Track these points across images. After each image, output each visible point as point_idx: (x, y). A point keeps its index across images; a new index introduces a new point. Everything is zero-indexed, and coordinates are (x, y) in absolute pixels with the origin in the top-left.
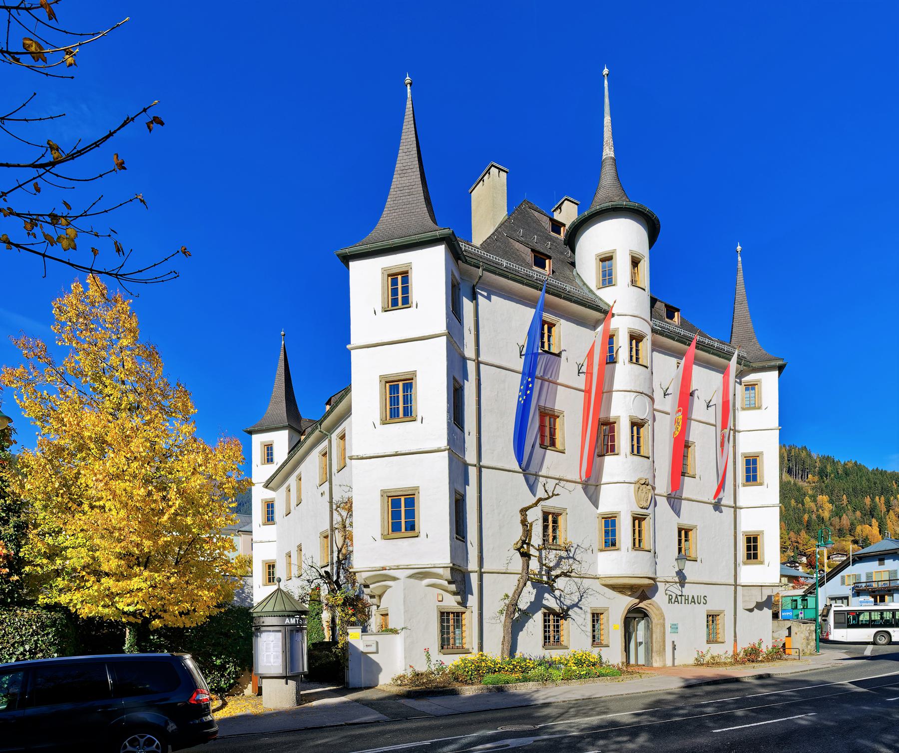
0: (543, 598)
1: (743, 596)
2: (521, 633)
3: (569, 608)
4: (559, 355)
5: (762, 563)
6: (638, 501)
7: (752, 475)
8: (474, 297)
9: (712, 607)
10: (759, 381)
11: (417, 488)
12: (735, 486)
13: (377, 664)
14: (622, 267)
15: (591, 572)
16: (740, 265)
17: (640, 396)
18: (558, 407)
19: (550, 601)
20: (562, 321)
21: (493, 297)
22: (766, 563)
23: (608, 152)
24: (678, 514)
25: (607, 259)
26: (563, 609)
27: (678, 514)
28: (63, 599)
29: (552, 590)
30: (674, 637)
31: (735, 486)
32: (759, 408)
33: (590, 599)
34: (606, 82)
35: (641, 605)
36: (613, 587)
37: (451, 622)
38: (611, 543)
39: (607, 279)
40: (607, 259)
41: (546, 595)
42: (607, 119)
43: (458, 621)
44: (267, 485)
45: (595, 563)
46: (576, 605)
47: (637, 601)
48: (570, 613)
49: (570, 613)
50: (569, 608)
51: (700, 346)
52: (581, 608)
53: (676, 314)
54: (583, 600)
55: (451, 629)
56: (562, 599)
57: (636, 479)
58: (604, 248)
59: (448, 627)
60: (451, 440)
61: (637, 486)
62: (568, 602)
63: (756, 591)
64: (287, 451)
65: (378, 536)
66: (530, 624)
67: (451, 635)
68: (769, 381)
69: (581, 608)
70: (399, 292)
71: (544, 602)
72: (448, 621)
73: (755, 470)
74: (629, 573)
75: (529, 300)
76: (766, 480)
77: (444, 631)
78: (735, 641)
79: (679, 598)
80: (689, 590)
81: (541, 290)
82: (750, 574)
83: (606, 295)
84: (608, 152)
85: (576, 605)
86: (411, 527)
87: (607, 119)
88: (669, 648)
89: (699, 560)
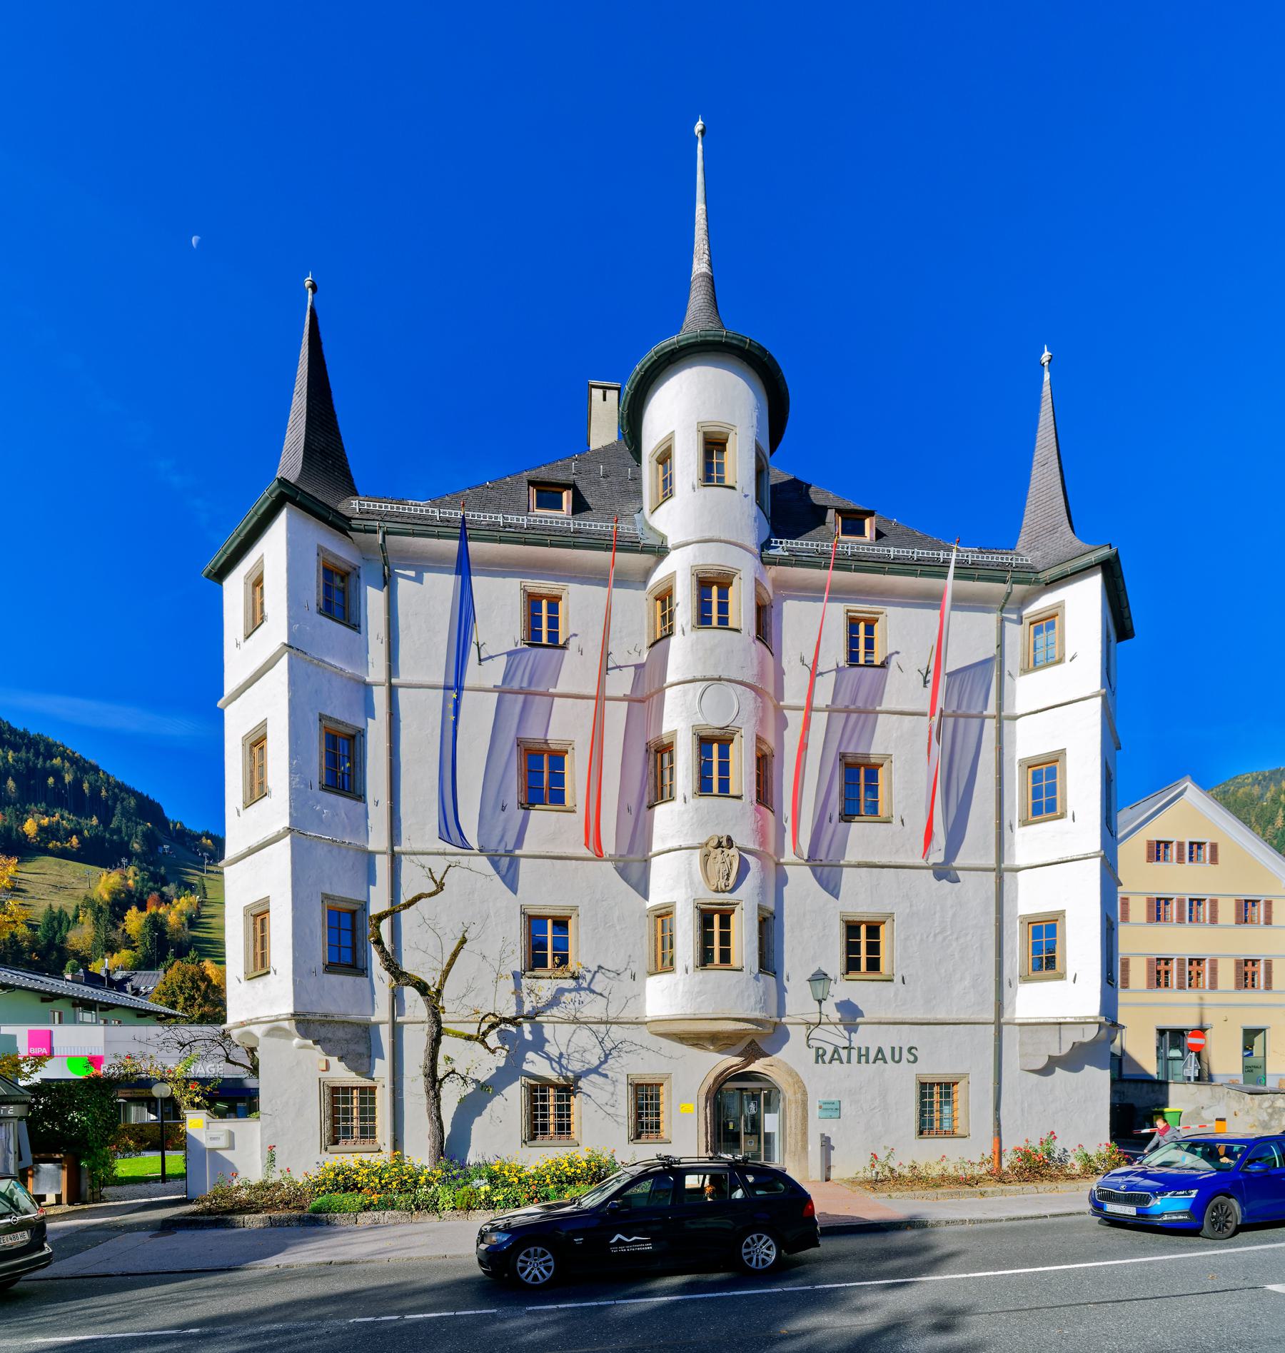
0: (524, 1060)
1: (1022, 1044)
2: (477, 1120)
3: (578, 1077)
4: (883, 665)
5: (1062, 977)
7: (1045, 799)
8: (388, 582)
9: (934, 1067)
10: (1061, 605)
11: (1062, 913)
12: (1000, 826)
13: (231, 1164)
15: (627, 1015)
16: (1046, 389)
17: (715, 687)
18: (876, 749)
19: (537, 1065)
20: (890, 610)
21: (427, 576)
22: (1070, 976)
23: (700, 266)
24: (514, 889)
26: (566, 1078)
27: (514, 889)
28: (36, 1078)
29: (539, 1044)
30: (831, 1128)
31: (1000, 826)
32: (1060, 661)
33: (625, 1059)
34: (700, 146)
35: (753, 1067)
36: (682, 1038)
37: (936, 1097)
38: (664, 962)
41: (530, 1055)
42: (700, 208)
43: (948, 1095)
45: (639, 996)
46: (595, 1071)
47: (737, 1060)
48: (580, 1084)
49: (580, 1084)
50: (578, 1077)
51: (964, 571)
52: (606, 1076)
53: (867, 522)
54: (610, 1061)
55: (936, 1107)
56: (564, 1062)
57: (704, 841)
59: (931, 1104)
60: (1104, 846)
62: (577, 1066)
63: (1049, 1036)
66: (496, 1105)
67: (936, 1115)
68: (1083, 603)
69: (606, 1076)
71: (526, 1067)
72: (931, 1095)
73: (1052, 789)
74: (708, 1011)
75: (500, 565)
76: (1072, 804)
77: (925, 1108)
78: (998, 1133)
79: (844, 1054)
80: (865, 1037)
81: (1005, 582)
82: (1034, 1001)
84: (700, 266)
85: (595, 1071)
86: (874, 965)
87: (700, 208)
88: (814, 1147)
89: (897, 979)
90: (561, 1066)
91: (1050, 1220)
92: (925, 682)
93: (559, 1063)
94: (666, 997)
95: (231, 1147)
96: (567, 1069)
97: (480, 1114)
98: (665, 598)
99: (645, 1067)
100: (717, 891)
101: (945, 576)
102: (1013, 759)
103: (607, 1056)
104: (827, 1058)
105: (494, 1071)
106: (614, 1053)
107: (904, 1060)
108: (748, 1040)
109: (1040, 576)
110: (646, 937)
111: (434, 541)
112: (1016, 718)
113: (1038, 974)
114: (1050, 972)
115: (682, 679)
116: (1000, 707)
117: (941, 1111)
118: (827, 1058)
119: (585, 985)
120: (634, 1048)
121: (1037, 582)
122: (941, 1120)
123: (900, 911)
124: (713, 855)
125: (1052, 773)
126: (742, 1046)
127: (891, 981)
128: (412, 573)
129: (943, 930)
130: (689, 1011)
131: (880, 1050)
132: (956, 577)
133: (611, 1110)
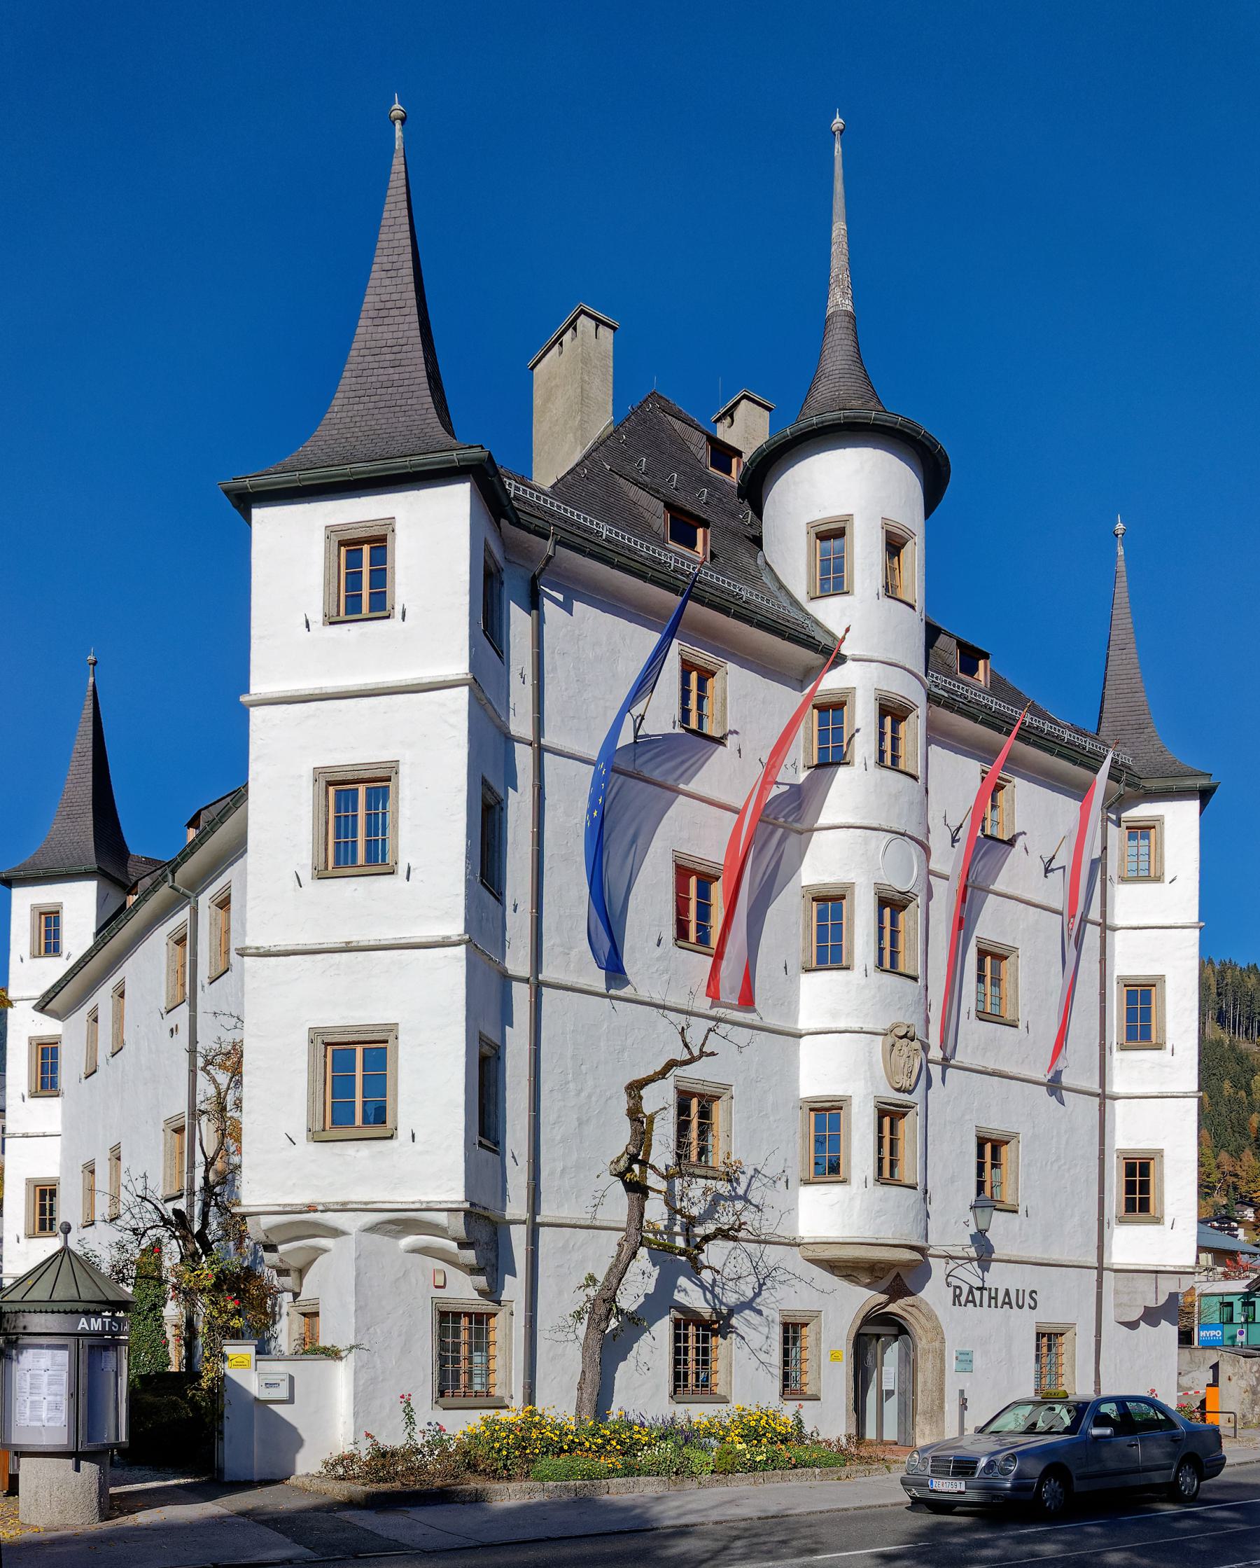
2: (622, 1365)
3: (732, 1312)
5: (1158, 1221)
6: (890, 1075)
7: (1141, 1022)
8: (533, 604)
9: (1050, 1314)
12: (1102, 1047)
14: (865, 553)
17: (900, 841)
19: (691, 1296)
21: (577, 606)
22: (1168, 1220)
23: (840, 300)
25: (832, 534)
29: (695, 1268)
30: (965, 1382)
31: (1102, 1047)
37: (464, 1336)
38: (829, 1168)
39: (832, 580)
40: (832, 534)
42: (839, 228)
44: (43, 1006)
48: (734, 1321)
49: (734, 1321)
50: (732, 1312)
52: (760, 1313)
55: (464, 1350)
58: (827, 509)
59: (456, 1348)
60: (471, 922)
61: (890, 1039)
62: (731, 1298)
63: (1145, 1283)
64: (94, 930)
65: (301, 1135)
67: (463, 1365)
68: (1180, 822)
69: (760, 1313)
70: (362, 576)
71: (678, 1297)
72: (456, 1334)
80: (999, 1277)
81: (1118, 782)
82: (1132, 1245)
83: (830, 614)
84: (840, 300)
85: (748, 1305)
87: (839, 228)
90: (715, 1296)
91: (890, 1508)
92: (954, 840)
93: (712, 1292)
94: (826, 1214)
95: (290, 1400)
96: (721, 1303)
97: (625, 1359)
98: (833, 709)
99: (787, 1298)
100: (898, 1090)
101: (1096, 771)
102: (1112, 974)
103: (761, 1286)
104: (963, 1299)
105: (642, 1299)
106: (769, 1283)
107: (1026, 1306)
108: (893, 1274)
109: (1142, 783)
110: (798, 1135)
111: (638, 583)
112: (1115, 929)
113: (1131, 1215)
114: (1143, 1215)
115: (865, 823)
116: (1104, 914)
117: (470, 1360)
118: (963, 1299)
119: (740, 1191)
120: (788, 1276)
121: (1136, 786)
122: (470, 1374)
123: (1025, 1133)
124: (898, 1045)
125: (1147, 997)
126: (886, 1283)
127: (1016, 1212)
128: (560, 597)
129: (1058, 1159)
130: (868, 1234)
131: (1007, 1293)
132: (1017, 738)
133: (763, 1357)
